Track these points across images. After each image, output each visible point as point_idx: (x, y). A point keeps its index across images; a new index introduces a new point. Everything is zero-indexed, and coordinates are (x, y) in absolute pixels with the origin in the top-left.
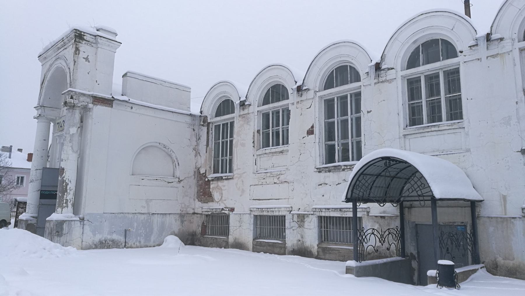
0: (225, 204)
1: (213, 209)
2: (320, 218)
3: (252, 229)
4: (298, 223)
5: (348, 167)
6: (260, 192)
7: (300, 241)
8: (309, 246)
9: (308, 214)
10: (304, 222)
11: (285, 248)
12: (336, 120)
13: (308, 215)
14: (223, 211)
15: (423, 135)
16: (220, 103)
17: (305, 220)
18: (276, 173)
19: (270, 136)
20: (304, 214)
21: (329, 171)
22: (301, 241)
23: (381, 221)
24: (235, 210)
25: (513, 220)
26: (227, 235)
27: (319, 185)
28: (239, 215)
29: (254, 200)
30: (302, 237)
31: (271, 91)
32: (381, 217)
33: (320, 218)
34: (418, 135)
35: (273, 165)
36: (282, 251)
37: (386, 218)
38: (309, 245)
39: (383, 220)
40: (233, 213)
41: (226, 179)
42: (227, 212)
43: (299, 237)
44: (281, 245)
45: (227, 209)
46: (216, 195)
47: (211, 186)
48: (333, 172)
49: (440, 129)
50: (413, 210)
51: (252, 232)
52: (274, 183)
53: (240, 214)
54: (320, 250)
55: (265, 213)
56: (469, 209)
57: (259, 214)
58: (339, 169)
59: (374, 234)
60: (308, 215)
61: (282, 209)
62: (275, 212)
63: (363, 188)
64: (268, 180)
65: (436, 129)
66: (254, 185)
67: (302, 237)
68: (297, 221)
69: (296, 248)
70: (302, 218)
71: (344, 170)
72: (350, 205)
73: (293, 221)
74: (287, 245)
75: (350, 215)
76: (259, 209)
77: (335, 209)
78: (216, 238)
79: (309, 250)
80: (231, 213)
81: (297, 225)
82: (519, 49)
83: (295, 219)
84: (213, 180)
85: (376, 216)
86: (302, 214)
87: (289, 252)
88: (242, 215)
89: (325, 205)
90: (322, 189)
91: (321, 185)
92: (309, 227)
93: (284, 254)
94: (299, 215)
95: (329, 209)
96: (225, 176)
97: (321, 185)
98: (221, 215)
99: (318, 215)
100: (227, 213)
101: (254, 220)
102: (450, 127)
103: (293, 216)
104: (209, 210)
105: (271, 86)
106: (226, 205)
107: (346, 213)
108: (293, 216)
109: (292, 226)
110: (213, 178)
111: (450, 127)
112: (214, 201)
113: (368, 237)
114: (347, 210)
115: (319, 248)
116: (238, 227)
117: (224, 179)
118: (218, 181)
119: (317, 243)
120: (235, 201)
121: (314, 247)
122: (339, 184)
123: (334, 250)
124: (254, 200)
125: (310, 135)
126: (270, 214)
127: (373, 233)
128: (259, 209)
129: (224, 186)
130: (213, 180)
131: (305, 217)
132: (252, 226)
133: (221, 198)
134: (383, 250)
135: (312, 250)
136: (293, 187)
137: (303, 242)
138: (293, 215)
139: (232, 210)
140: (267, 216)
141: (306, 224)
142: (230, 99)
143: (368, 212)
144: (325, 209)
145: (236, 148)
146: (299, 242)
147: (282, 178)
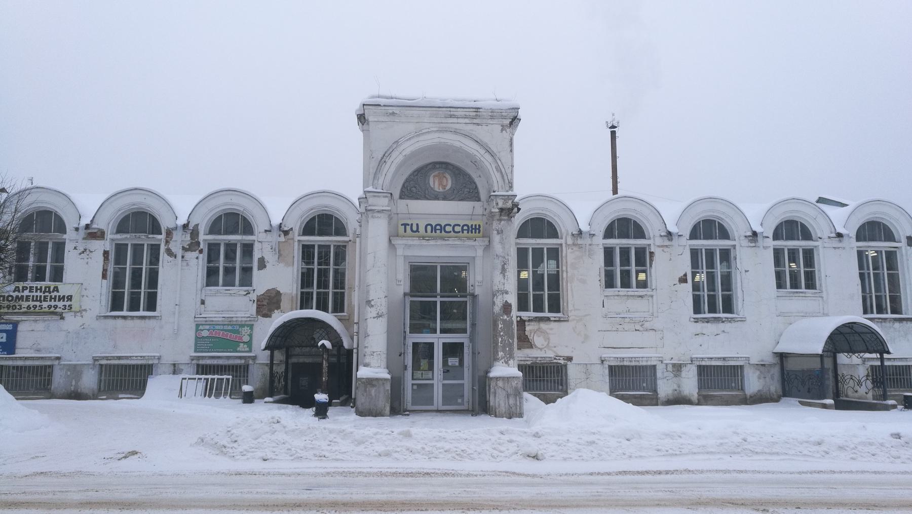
0: (554, 352)
1: (537, 358)
2: (699, 367)
3: (608, 380)
4: (673, 372)
5: (729, 320)
6: (613, 339)
7: (676, 390)
8: (688, 394)
9: (685, 364)
10: (681, 371)
11: (657, 399)
12: (144, 267)
13: (685, 365)
14: (555, 361)
15: (791, 298)
16: (526, 219)
17: (682, 369)
18: (639, 319)
19: (356, 276)
20: (681, 364)
21: (707, 322)
22: (678, 391)
23: (762, 368)
24: (573, 359)
25: (857, 366)
26: (140, 389)
27: (695, 335)
28: (585, 366)
29: (604, 347)
30: (679, 387)
31: (318, 222)
32: (762, 365)
33: (699, 367)
34: (788, 298)
35: (627, 309)
36: (654, 402)
37: (766, 365)
38: (768, 394)
39: (763, 367)
40: (572, 362)
41: (555, 321)
42: (562, 362)
43: (675, 387)
44: (651, 396)
45: (562, 358)
46: (538, 340)
47: (527, 328)
48: (711, 323)
49: (806, 295)
50: (789, 359)
51: (608, 384)
52: (636, 330)
53: (586, 364)
54: (701, 397)
55: (626, 363)
56: (831, 358)
57: (616, 364)
58: (719, 321)
59: (798, 379)
60: (685, 365)
61: (652, 359)
62: (640, 362)
63: (279, 338)
64: (626, 327)
65: (803, 295)
66: (604, 331)
67: (679, 387)
68: (671, 371)
69: (671, 397)
70: (678, 368)
71: (723, 322)
72: (268, 352)
73: (667, 371)
74: (659, 396)
75: (879, 363)
76: (619, 359)
77: (718, 358)
78: (544, 394)
79: (687, 398)
80: (569, 363)
81: (672, 375)
82: (735, 245)
83: (670, 368)
84: (529, 321)
85: (757, 365)
86: (678, 364)
87: (663, 403)
88: (588, 366)
89: (703, 354)
90: (700, 339)
91: (698, 335)
92: (687, 376)
93: (657, 405)
94: (674, 365)
95: (712, 358)
96: (555, 317)
97: (698, 335)
98: (552, 365)
99: (698, 364)
100: (563, 363)
101: (197, 367)
102: (814, 295)
103: (667, 365)
104: (528, 359)
105: (225, 213)
106: (557, 353)
107: (730, 362)
108: (667, 365)
109: (665, 376)
110: (531, 318)
111: (814, 295)
112: (534, 347)
113: (847, 381)
114: (731, 359)
115: (699, 395)
116: (583, 380)
117: (552, 321)
118: (541, 323)
119: (697, 391)
120: (573, 348)
121: (693, 395)
122: (717, 334)
123: (718, 396)
124: (604, 347)
125: (682, 283)
126: (633, 364)
127: (796, 378)
128: (617, 358)
129: (551, 329)
130: (529, 321)
131: (682, 366)
132: (608, 377)
133: (548, 344)
134: (764, 393)
135: (692, 398)
136: (662, 335)
137: (680, 391)
138: (667, 365)
139: (570, 359)
140: (628, 366)
141: (683, 374)
142: (546, 218)
143: (749, 360)
144: (708, 358)
145: (571, 283)
146: (675, 392)
147: (647, 325)
